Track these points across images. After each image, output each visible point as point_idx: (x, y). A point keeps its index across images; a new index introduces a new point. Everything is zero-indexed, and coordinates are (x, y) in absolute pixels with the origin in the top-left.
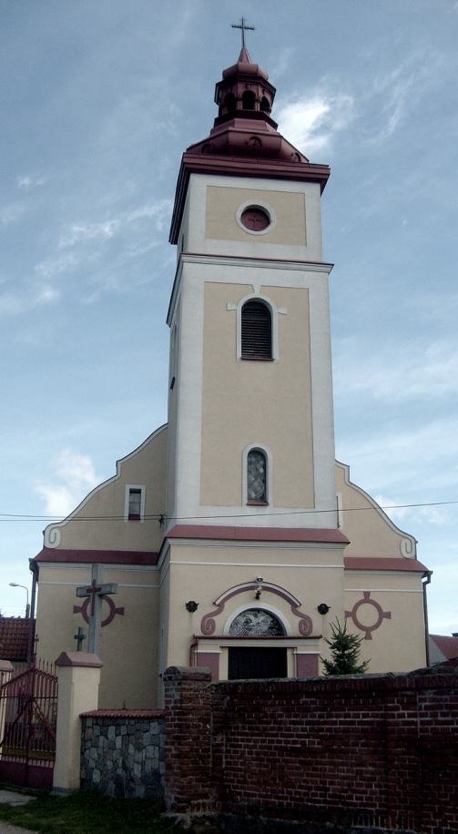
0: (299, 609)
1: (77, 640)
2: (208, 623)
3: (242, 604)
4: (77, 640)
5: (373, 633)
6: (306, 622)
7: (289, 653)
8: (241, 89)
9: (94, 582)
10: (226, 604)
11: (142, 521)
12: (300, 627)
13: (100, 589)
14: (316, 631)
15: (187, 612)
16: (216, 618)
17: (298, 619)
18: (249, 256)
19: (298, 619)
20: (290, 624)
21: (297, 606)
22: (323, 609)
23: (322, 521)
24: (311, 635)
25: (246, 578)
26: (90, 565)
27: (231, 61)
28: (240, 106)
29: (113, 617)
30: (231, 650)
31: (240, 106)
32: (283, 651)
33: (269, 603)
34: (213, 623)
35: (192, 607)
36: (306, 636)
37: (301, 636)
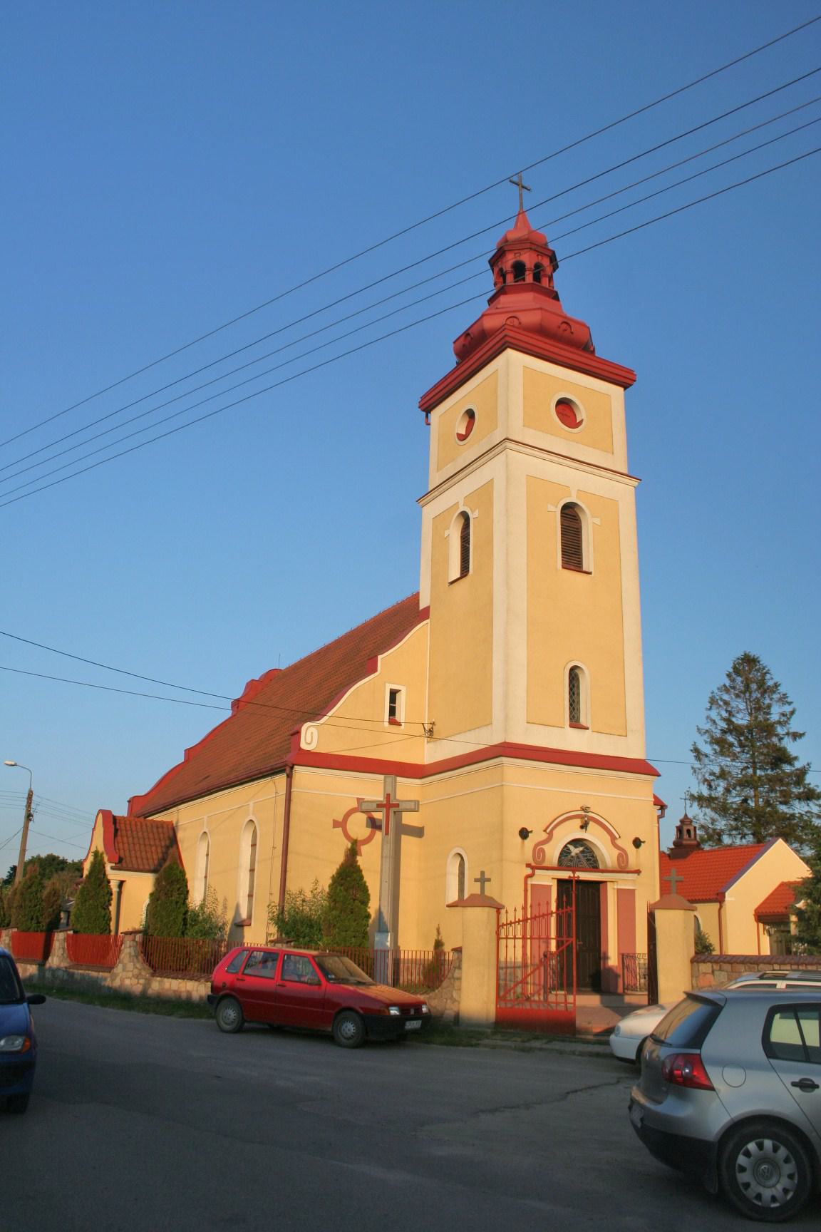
0: (618, 842)
1: (479, 884)
2: (539, 851)
3: (571, 831)
4: (479, 884)
5: (355, 805)
6: (623, 856)
7: (609, 885)
8: (510, 259)
9: (388, 797)
10: (555, 832)
11: (402, 727)
12: (618, 859)
13: (397, 805)
14: (632, 863)
15: (519, 839)
16: (545, 847)
17: (617, 852)
18: (564, 454)
19: (617, 852)
20: (607, 854)
21: (615, 838)
22: (637, 843)
23: (632, 749)
24: (627, 870)
25: (574, 805)
26: (382, 777)
27: (507, 229)
28: (529, 278)
29: (343, 819)
30: (560, 882)
31: (529, 278)
32: (597, 885)
33: (594, 836)
34: (543, 851)
35: (524, 834)
36: (623, 868)
37: (619, 869)
